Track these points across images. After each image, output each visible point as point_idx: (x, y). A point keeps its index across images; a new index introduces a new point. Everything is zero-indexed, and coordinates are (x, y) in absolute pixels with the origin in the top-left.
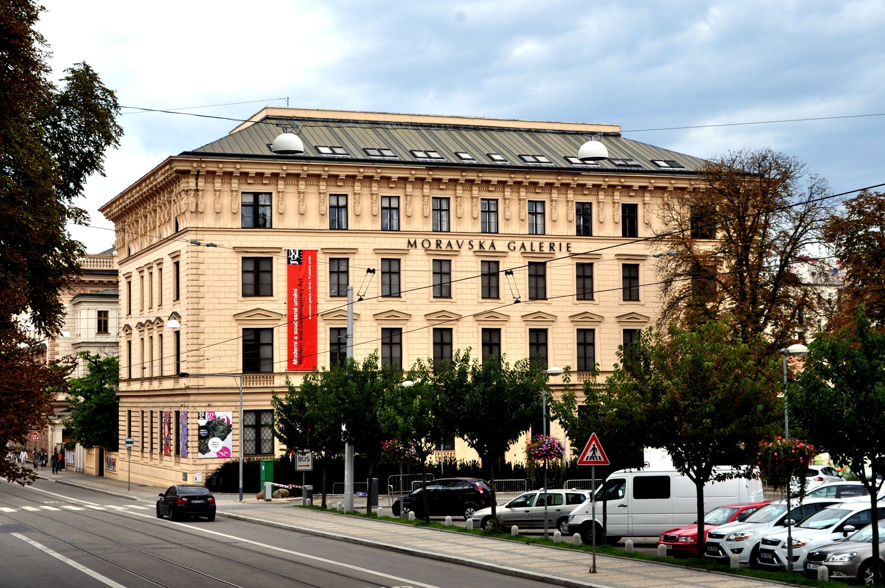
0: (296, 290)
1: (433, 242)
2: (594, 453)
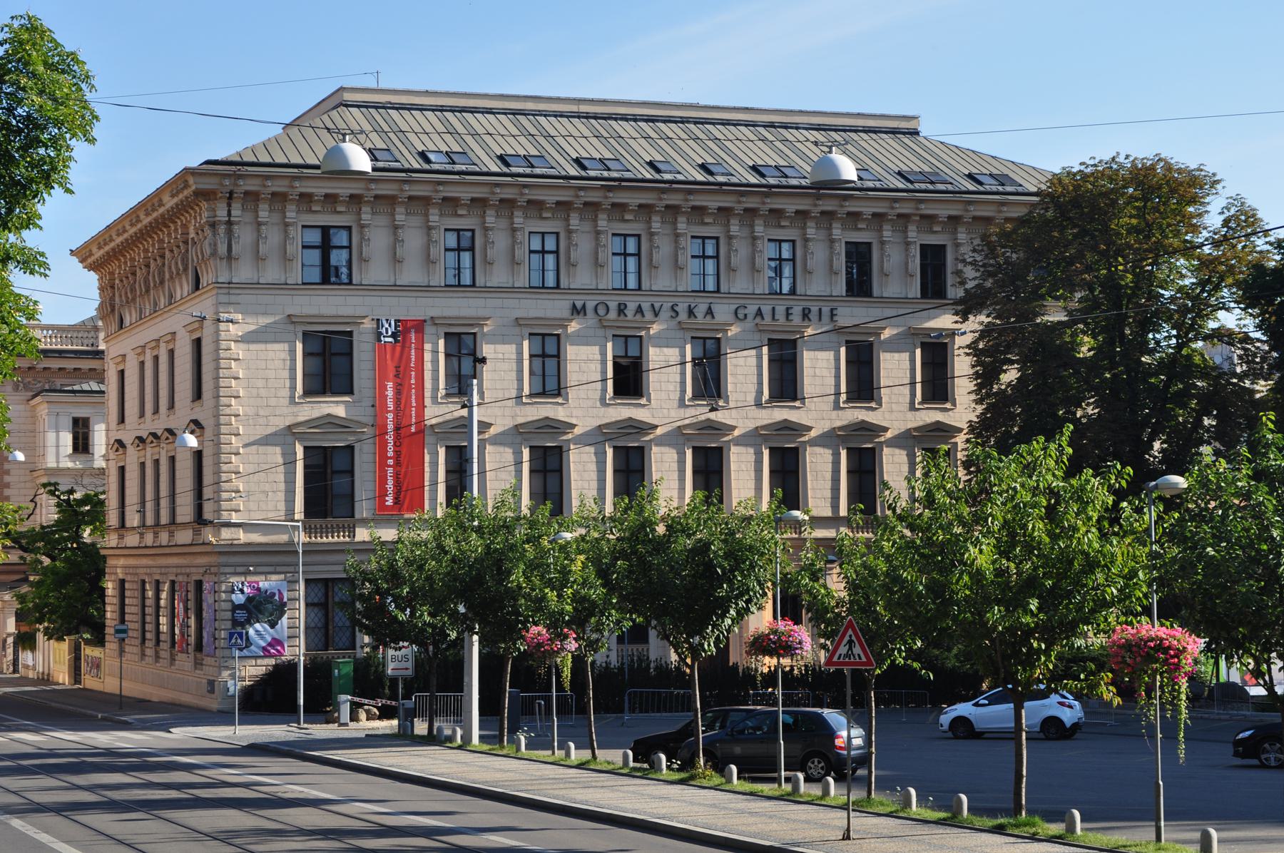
0: (390, 384)
1: (613, 305)
2: (850, 648)
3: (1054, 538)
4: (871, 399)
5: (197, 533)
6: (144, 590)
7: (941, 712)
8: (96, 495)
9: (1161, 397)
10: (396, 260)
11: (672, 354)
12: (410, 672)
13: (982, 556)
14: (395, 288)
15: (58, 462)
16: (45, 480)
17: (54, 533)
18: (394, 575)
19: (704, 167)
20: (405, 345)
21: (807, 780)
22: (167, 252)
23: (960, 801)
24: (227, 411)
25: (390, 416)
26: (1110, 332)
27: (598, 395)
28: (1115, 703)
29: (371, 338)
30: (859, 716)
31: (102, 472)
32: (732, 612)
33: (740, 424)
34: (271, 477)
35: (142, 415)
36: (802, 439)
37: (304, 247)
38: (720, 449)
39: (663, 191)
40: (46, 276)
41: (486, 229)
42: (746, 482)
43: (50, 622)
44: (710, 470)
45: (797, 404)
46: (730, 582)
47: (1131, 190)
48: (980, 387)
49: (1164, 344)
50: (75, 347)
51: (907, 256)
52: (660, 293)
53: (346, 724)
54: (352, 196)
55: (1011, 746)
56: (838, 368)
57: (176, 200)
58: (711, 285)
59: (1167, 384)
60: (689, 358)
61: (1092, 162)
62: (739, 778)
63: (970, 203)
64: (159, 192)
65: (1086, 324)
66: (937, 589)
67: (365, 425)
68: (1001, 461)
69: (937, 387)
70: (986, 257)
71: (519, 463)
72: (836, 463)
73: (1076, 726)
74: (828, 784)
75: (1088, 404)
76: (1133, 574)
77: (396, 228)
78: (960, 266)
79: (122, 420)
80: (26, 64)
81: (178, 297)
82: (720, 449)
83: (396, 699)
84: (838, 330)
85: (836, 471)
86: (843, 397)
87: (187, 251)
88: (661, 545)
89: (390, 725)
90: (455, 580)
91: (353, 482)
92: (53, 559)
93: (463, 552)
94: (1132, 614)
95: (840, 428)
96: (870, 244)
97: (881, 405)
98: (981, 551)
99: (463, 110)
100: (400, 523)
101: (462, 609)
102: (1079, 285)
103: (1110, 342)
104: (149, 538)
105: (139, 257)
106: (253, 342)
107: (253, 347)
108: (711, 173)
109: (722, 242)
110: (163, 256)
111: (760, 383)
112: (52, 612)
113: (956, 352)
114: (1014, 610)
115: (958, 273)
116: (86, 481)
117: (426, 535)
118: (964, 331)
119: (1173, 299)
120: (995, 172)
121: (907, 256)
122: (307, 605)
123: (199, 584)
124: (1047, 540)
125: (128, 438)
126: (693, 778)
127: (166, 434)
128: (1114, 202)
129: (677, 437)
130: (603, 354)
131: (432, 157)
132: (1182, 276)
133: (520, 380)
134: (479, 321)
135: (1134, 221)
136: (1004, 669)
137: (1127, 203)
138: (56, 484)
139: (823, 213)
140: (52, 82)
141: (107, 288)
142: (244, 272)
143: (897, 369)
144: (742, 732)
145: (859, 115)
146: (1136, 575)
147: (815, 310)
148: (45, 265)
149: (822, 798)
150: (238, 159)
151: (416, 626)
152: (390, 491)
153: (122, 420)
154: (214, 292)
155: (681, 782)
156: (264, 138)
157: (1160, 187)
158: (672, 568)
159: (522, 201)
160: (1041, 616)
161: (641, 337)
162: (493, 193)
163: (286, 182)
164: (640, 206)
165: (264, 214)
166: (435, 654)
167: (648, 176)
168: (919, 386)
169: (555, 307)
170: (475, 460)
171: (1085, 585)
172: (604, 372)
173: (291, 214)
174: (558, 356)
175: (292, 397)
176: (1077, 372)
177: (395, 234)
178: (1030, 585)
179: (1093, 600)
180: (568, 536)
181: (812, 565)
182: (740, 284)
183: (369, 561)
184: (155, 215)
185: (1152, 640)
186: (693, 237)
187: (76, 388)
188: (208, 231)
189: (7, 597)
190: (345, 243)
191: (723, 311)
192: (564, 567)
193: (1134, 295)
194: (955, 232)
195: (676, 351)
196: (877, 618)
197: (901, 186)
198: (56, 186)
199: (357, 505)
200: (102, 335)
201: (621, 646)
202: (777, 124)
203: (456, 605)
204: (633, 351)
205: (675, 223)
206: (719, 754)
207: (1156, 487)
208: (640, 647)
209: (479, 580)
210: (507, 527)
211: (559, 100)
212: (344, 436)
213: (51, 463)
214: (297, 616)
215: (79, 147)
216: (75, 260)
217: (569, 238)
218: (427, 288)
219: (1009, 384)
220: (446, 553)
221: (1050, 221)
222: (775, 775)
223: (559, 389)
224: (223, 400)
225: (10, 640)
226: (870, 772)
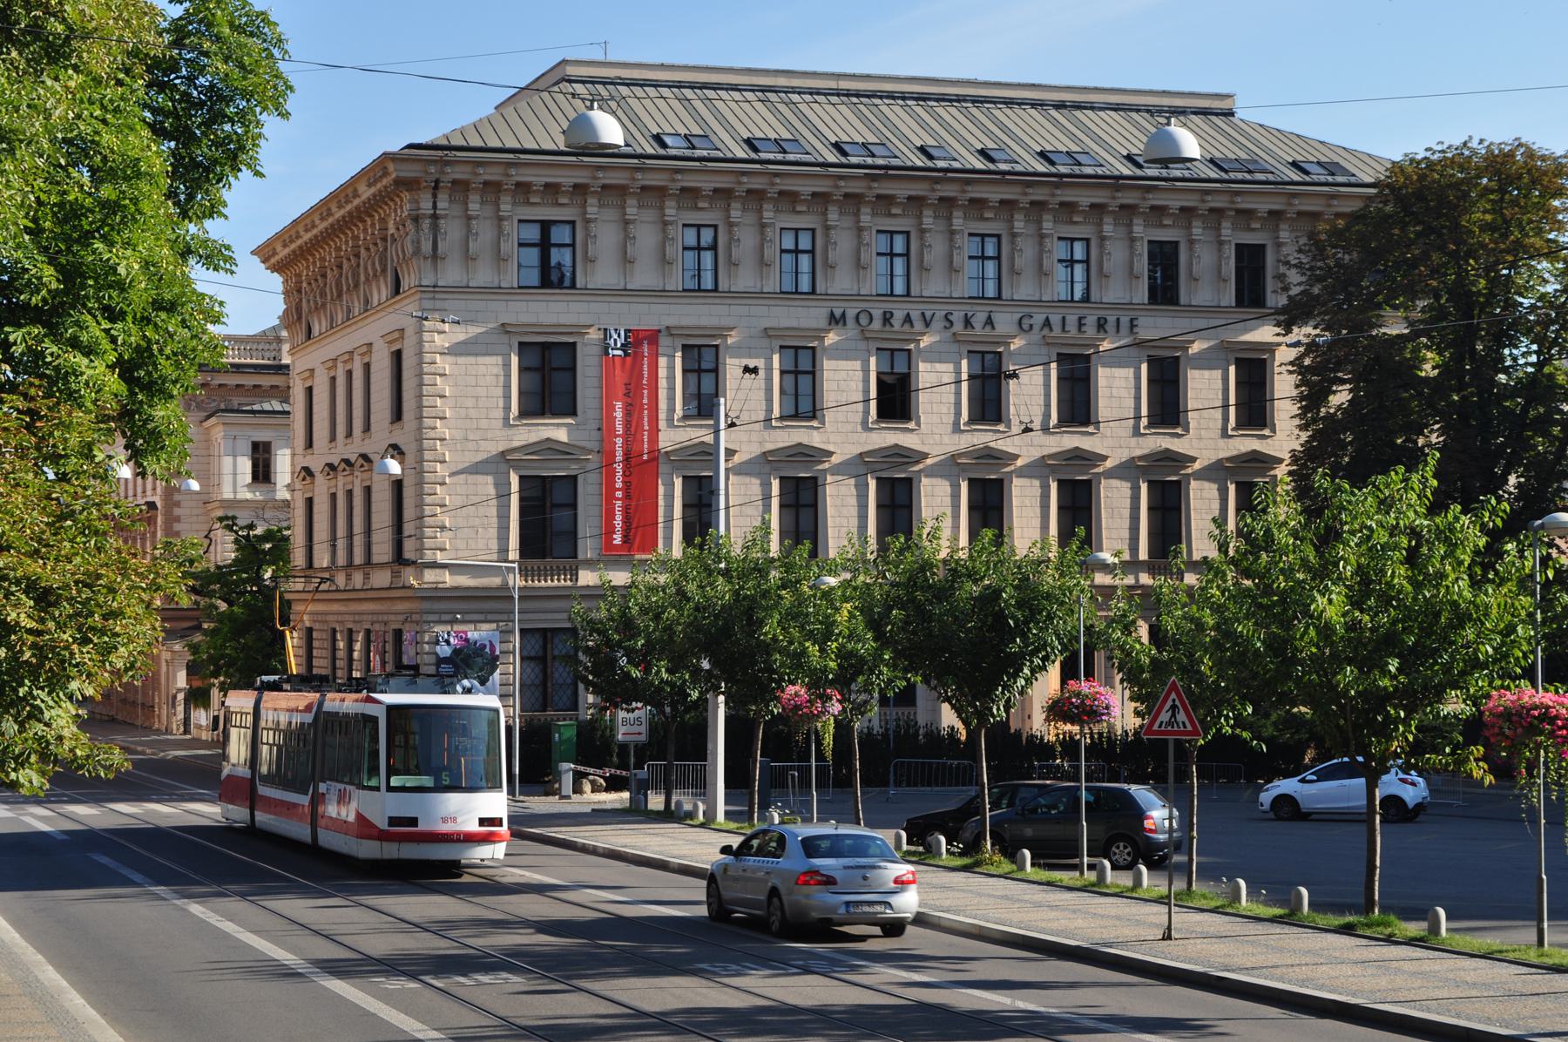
0: (619, 405)
1: (877, 314)
2: (1173, 715)
3: (1418, 587)
4: (1176, 424)
5: (396, 575)
6: (334, 640)
7: (1260, 789)
8: (280, 530)
9: (1519, 426)
10: (626, 261)
11: (945, 371)
12: (643, 738)
13: (1331, 605)
14: (625, 292)
15: (235, 492)
16: (220, 513)
17: (231, 573)
18: (627, 625)
19: (983, 153)
20: (638, 357)
21: (1113, 868)
22: (363, 251)
23: (1299, 895)
24: (432, 434)
25: (619, 441)
26: (1458, 346)
27: (859, 418)
28: (1487, 782)
29: (597, 350)
30: (1176, 796)
31: (286, 504)
32: (1026, 671)
33: (1023, 452)
34: (482, 510)
35: (333, 438)
36: (1096, 470)
37: (520, 245)
38: (1000, 482)
39: (937, 181)
40: (232, 272)
41: (731, 225)
42: (1030, 522)
43: (226, 676)
44: (988, 505)
45: (1091, 429)
46: (1024, 636)
47: (1485, 181)
48: (1304, 410)
49: (1521, 361)
50: (254, 361)
51: (1220, 257)
52: (932, 300)
53: (568, 797)
54: (576, 186)
55: (1363, 828)
56: (1138, 388)
57: (373, 190)
58: (991, 291)
59: (1525, 410)
60: (965, 376)
61: (1439, 148)
62: (1033, 865)
63: (1295, 195)
64: (354, 180)
65: (1430, 338)
66: (1278, 646)
67: (590, 452)
68: (1354, 494)
69: (1253, 410)
70: (1314, 258)
71: (767, 498)
72: (1135, 499)
73: (1420, 807)
74: (1140, 873)
75: (1432, 431)
76: (1511, 629)
77: (627, 223)
78: (1282, 269)
79: (309, 444)
80: (210, 25)
81: (375, 302)
82: (1000, 482)
83: (627, 769)
84: (1140, 344)
85: (1135, 508)
86: (1144, 421)
87: (386, 249)
88: (943, 593)
89: (621, 798)
90: (698, 631)
91: (575, 515)
92: (230, 604)
93: (709, 599)
94: (1510, 677)
95: (1140, 458)
96: (1177, 243)
97: (1188, 431)
98: (1330, 601)
99: (704, 86)
100: (631, 565)
101: (706, 665)
102: (1423, 292)
103: (1458, 359)
104: (341, 580)
105: (333, 255)
106: (461, 355)
107: (461, 360)
108: (992, 160)
109: (1004, 240)
110: (357, 256)
111: (1048, 405)
112: (229, 665)
113: (1277, 370)
114: (1369, 671)
115: (1280, 277)
116: (268, 515)
117: (663, 579)
118: (1284, 347)
119: (1533, 308)
120: (1324, 159)
121: (1220, 257)
122: (522, 659)
123: (398, 634)
124: (1410, 588)
125: (316, 464)
126: (978, 864)
127: (361, 461)
128: (1466, 195)
129: (951, 467)
130: (866, 371)
131: (668, 140)
132: (1546, 281)
133: (769, 400)
134: (722, 332)
135: (1488, 217)
136: (1351, 739)
137: (1481, 196)
138: (234, 518)
139: (1122, 207)
140: (240, 46)
141: (293, 293)
142: (452, 274)
143: (1207, 390)
144: (1034, 811)
145: (1165, 93)
146: (1514, 630)
147: (1111, 319)
148: (230, 260)
149: (1133, 889)
150: (445, 142)
151: (652, 684)
152: (618, 528)
153: (309, 444)
154: (417, 296)
155: (965, 869)
156: (475, 118)
157: (1520, 177)
158: (956, 618)
159: (772, 192)
160: (1402, 679)
161: (909, 351)
162: (740, 183)
163: (500, 170)
164: (910, 198)
165: (474, 207)
166: (674, 717)
167: (919, 163)
168: (1232, 410)
169: (809, 316)
170: (722, 492)
171: (1453, 643)
172: (866, 391)
173: (506, 207)
174: (813, 373)
175: (506, 419)
176: (1420, 394)
177: (625, 229)
178: (1388, 642)
179: (1464, 661)
180: (832, 581)
181: (1124, 616)
182: (1025, 289)
183: (598, 609)
184: (349, 207)
185: (1536, 707)
186: (970, 235)
187: (256, 407)
188: (410, 226)
189: (177, 647)
190: (568, 241)
191: (1005, 321)
192: (827, 617)
193: (1488, 303)
194: (1276, 230)
195: (950, 367)
196: (1201, 679)
197: (1213, 175)
198: (243, 168)
199: (580, 542)
200: (286, 347)
201: (887, 710)
202: (1069, 104)
203: (699, 659)
204: (900, 368)
205: (949, 218)
206: (1007, 836)
207: (1542, 526)
208: (906, 710)
209: (726, 631)
210: (759, 571)
211: (814, 75)
212: (566, 464)
213: (227, 494)
214: (511, 669)
215: (270, 123)
216: (256, 259)
217: (827, 235)
218: (662, 293)
219: (1339, 408)
220: (688, 599)
221: (1391, 216)
222: (1077, 861)
223: (814, 410)
224: (427, 422)
225: (181, 696)
226: (1191, 860)
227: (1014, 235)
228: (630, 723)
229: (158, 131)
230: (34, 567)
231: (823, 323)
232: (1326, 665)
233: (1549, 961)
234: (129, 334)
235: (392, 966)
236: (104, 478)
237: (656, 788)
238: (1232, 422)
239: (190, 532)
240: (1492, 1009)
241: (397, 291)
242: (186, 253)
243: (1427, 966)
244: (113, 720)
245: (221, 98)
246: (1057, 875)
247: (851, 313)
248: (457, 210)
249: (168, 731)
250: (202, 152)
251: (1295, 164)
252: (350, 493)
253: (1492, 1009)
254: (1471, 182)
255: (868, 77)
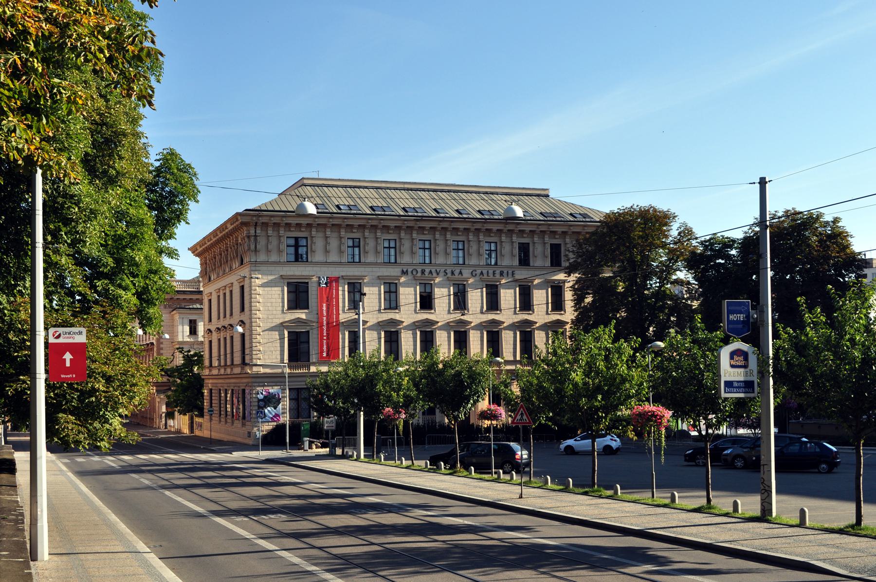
1: (419, 270)
3: (608, 369)
4: (530, 310)
5: (243, 369)
7: (560, 443)
10: (327, 252)
11: (445, 291)
13: (577, 376)
14: (326, 263)
16: (177, 346)
18: (327, 386)
20: (331, 289)
26: (631, 281)
27: (413, 309)
29: (316, 285)
30: (525, 446)
31: (202, 343)
35: (219, 318)
38: (465, 332)
41: (365, 238)
42: (477, 346)
44: (461, 341)
48: (576, 304)
52: (439, 265)
55: (591, 457)
56: (515, 297)
58: (461, 262)
59: (656, 303)
63: (571, 226)
69: (558, 305)
71: (380, 338)
72: (515, 337)
73: (618, 449)
76: (642, 384)
77: (327, 237)
79: (210, 320)
82: (465, 332)
84: (516, 281)
85: (515, 341)
88: (441, 373)
89: (325, 451)
92: (181, 380)
99: (355, 187)
100: (329, 364)
101: (356, 401)
103: (631, 285)
104: (222, 371)
105: (226, 248)
107: (266, 289)
108: (461, 213)
111: (482, 303)
115: (566, 256)
116: (195, 347)
117: (340, 369)
119: (657, 266)
123: (244, 391)
125: (213, 328)
126: (455, 472)
129: (447, 327)
130: (415, 291)
131: (342, 207)
133: (380, 302)
134: (362, 277)
136: (587, 425)
140: (181, 176)
142: (262, 257)
143: (540, 297)
145: (524, 189)
147: (505, 272)
148: (177, 255)
153: (210, 320)
165: (270, 232)
169: (394, 271)
172: (416, 299)
176: (617, 298)
178: (598, 389)
180: (401, 369)
182: (474, 261)
188: (246, 239)
191: (466, 273)
193: (641, 265)
194: (565, 238)
196: (533, 404)
200: (201, 284)
202: (489, 192)
204: (428, 290)
205: (445, 235)
211: (395, 182)
213: (180, 339)
215: (192, 204)
227: (469, 241)
228: (329, 422)
229: (150, 208)
230: (105, 368)
231: (399, 274)
232: (577, 396)
233: (655, 503)
234: (140, 282)
235: (238, 512)
236: (131, 335)
237: (339, 446)
238: (550, 308)
239: (166, 354)
240: (633, 520)
241: (242, 263)
242: (161, 252)
243: (612, 506)
244: (138, 424)
245: (174, 196)
246: (483, 476)
247: (410, 270)
248: (264, 233)
249: (159, 428)
250: (166, 215)
251: (571, 214)
252: (225, 339)
253: (633, 520)
254: (634, 221)
255: (415, 183)
